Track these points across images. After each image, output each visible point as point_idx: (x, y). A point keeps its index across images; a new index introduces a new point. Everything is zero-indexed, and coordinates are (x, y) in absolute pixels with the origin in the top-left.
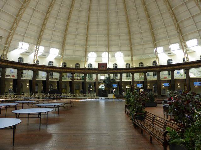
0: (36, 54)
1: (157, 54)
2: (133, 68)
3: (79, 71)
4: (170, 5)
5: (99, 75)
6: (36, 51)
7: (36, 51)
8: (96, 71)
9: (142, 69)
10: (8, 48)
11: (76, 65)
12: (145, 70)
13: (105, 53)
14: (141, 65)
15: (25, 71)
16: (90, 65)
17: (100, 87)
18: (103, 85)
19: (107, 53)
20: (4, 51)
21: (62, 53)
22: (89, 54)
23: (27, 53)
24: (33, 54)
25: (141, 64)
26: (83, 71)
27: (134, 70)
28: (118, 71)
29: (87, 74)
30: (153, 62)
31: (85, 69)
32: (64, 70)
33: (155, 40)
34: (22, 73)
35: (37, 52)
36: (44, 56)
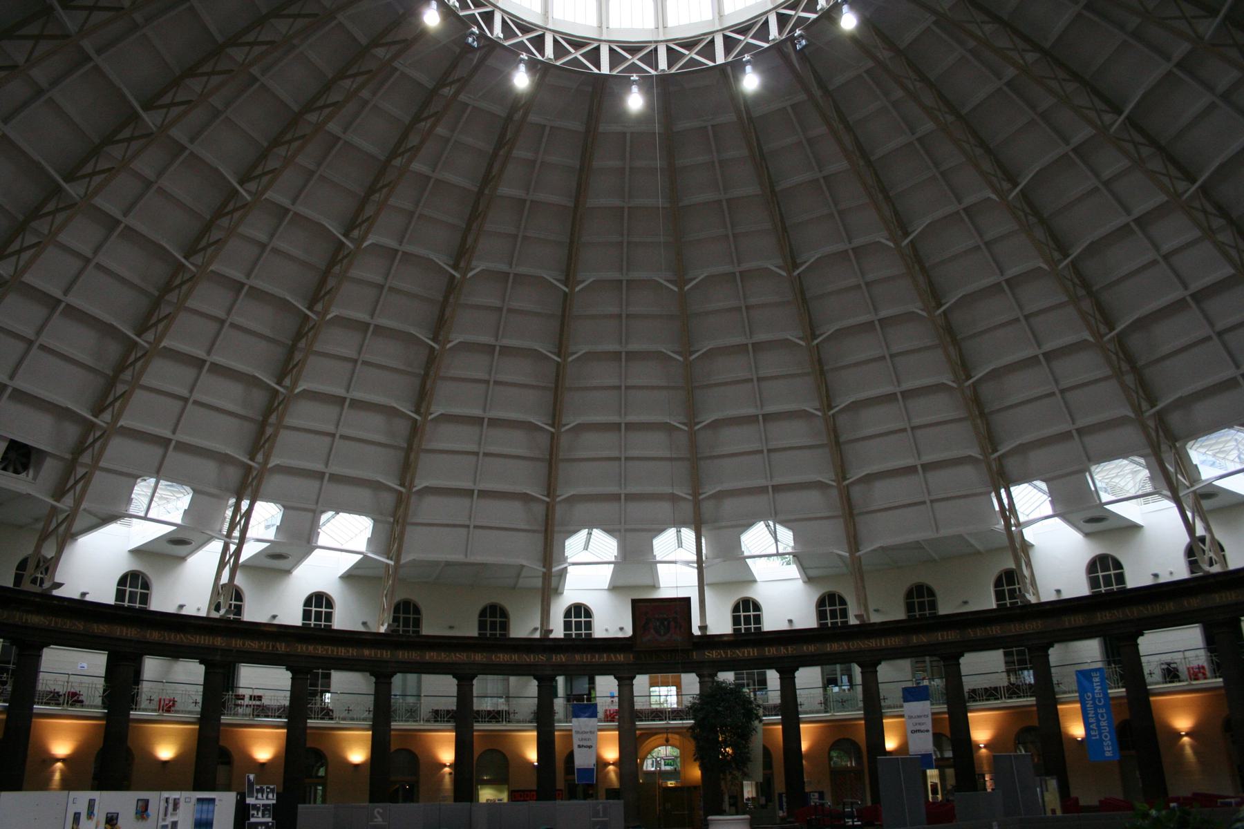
0: (233, 548)
1: (1018, 524)
2: (866, 630)
3: (503, 658)
4: (931, 284)
5: (641, 681)
6: (229, 535)
7: (229, 535)
8: (621, 658)
10: (71, 517)
11: (483, 613)
12: (951, 636)
15: (152, 666)
16: (579, 612)
17: (649, 766)
20: (44, 537)
22: (568, 543)
23: (177, 545)
24: (216, 547)
27: (873, 643)
28: (770, 651)
29: (560, 680)
31: (545, 645)
32: (402, 655)
34: (137, 677)
35: (236, 533)
36: (277, 562)
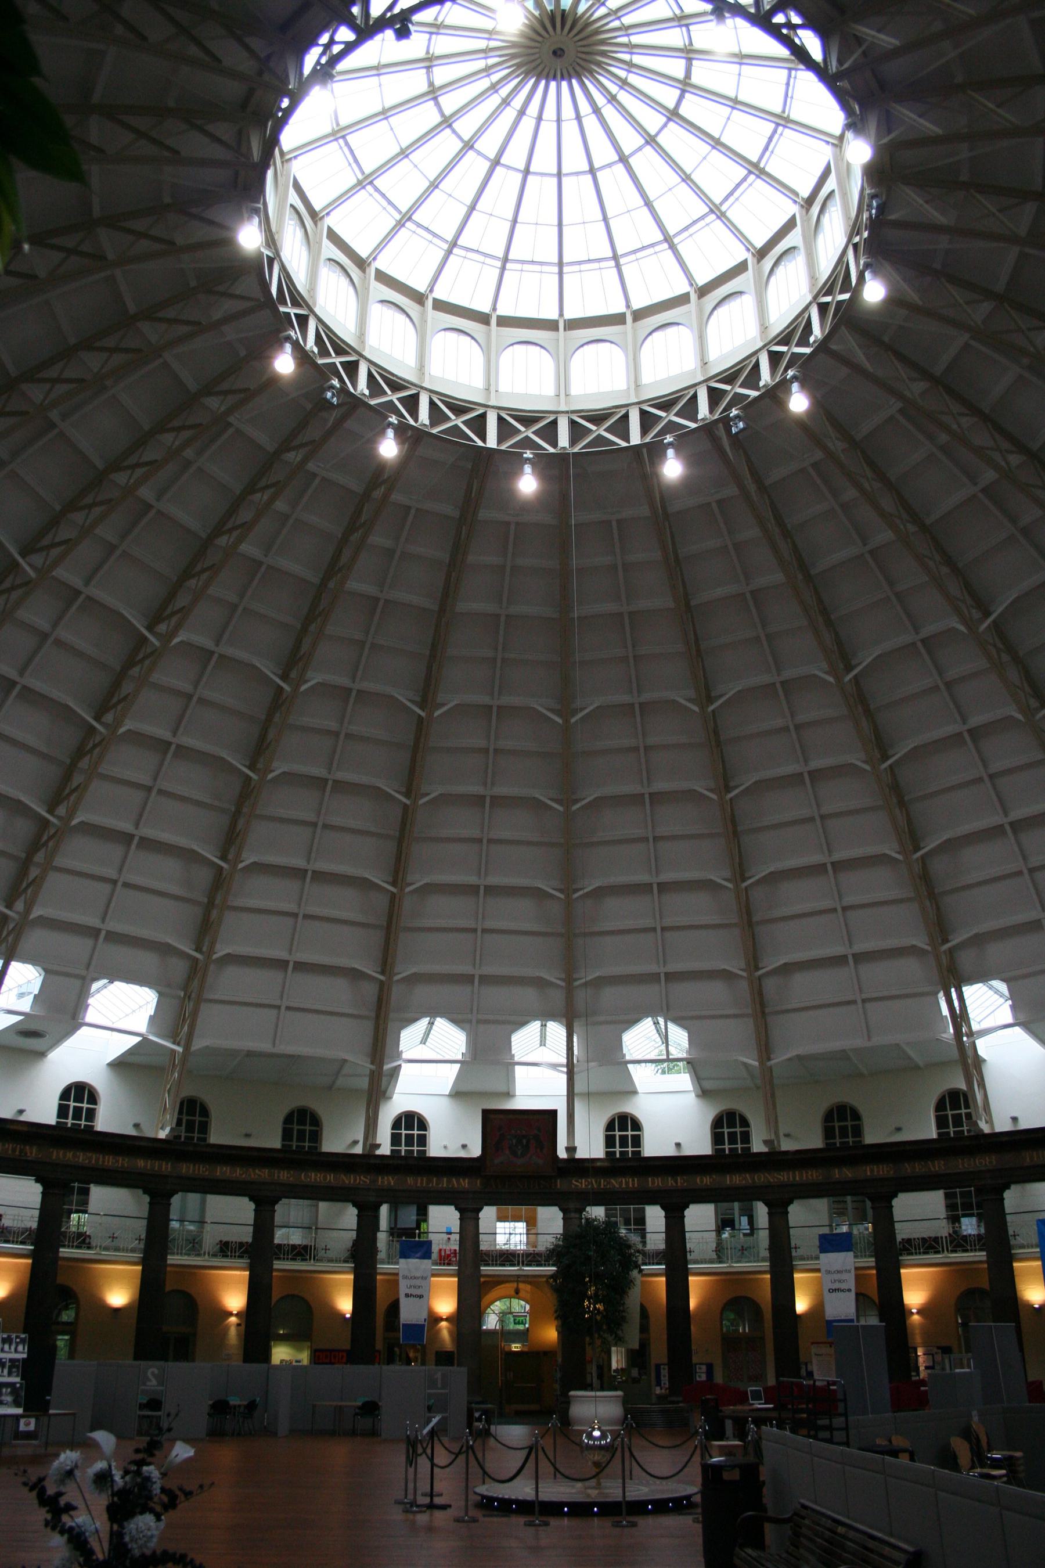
1: (971, 1034)
2: (775, 1159)
3: (315, 1177)
8: (465, 1183)
9: (854, 1169)
11: (288, 1119)
19: (556, 1031)
21: (180, 1012)
26: (348, 1180)
27: (784, 1177)
28: (655, 1183)
31: (368, 1162)
32: (186, 1169)
33: (940, 928)
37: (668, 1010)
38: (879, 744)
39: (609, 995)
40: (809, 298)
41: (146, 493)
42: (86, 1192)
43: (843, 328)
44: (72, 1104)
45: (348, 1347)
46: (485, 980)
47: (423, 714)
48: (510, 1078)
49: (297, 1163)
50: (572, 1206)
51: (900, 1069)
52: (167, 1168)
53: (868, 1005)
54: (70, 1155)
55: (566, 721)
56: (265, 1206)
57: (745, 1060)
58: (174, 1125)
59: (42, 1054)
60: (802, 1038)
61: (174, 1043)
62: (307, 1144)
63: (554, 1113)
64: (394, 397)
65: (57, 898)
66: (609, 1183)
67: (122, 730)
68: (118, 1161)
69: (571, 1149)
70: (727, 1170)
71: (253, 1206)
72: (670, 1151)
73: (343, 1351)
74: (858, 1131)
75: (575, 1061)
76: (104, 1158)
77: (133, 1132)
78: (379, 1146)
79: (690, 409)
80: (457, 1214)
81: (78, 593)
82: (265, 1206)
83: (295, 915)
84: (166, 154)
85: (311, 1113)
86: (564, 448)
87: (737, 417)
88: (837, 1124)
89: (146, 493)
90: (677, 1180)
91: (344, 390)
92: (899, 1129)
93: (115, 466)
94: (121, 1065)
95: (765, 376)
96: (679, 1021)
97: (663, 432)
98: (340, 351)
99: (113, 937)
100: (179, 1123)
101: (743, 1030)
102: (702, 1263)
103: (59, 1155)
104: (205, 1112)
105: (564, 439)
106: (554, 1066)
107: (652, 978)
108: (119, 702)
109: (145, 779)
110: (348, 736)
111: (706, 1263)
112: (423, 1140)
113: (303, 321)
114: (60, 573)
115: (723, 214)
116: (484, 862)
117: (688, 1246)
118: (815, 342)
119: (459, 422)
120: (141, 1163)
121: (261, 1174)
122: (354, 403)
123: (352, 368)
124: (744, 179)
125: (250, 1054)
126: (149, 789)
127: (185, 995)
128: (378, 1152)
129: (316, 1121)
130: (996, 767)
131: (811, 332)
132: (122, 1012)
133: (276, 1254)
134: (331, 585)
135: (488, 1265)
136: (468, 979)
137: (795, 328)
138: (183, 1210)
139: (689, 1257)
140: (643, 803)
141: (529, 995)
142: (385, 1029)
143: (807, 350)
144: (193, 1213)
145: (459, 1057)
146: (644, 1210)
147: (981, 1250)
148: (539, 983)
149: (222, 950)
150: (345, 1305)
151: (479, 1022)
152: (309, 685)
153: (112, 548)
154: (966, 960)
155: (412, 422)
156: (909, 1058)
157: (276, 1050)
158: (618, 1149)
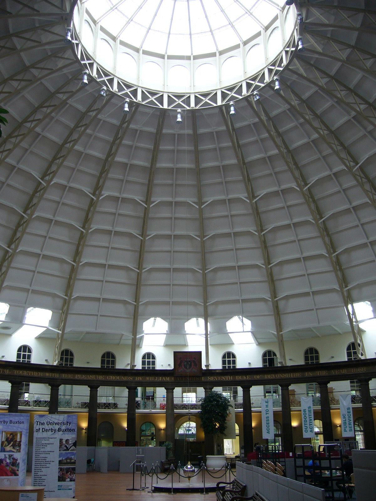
1: (357, 322)
2: (285, 369)
3: (112, 378)
8: (168, 379)
9: (317, 372)
11: (103, 356)
12: (324, 373)
13: (194, 320)
14: (312, 357)
16: (149, 356)
17: (181, 431)
18: (193, 424)
19: (202, 321)
21: (61, 319)
25: (229, 357)
26: (125, 379)
27: (286, 376)
28: (239, 378)
30: (349, 348)
31: (133, 372)
32: (64, 376)
33: (344, 281)
37: (243, 313)
38: (319, 213)
39: (221, 308)
40: (282, 49)
41: (38, 129)
42: (29, 385)
43: (295, 59)
44: (22, 353)
45: (125, 440)
46: (174, 303)
47: (146, 206)
48: (185, 340)
49: (107, 372)
50: (208, 387)
51: (333, 335)
52: (57, 376)
53: (318, 311)
54: (21, 372)
55: (200, 207)
56: (94, 389)
57: (273, 332)
58: (59, 360)
59: (10, 335)
60: (292, 324)
61: (59, 330)
62: (110, 365)
63: (200, 353)
64: (128, 91)
65: (13, 277)
66: (221, 378)
67: (34, 216)
68: (39, 374)
69: (207, 366)
70: (270, 372)
71: (89, 389)
72: (247, 366)
73: (124, 442)
74: (317, 358)
75: (209, 333)
76: (34, 373)
77: (45, 363)
78: (135, 366)
79: (239, 91)
80: (165, 391)
81: (15, 167)
82: (94, 389)
83: (102, 281)
84: (35, 12)
85: (112, 354)
86: (193, 107)
87: (256, 94)
88: (309, 355)
89: (38, 129)
90: (248, 378)
91: (108, 90)
92: (333, 357)
93: (25, 121)
94: (40, 338)
95: (267, 79)
96: (247, 317)
97: (229, 100)
98: (106, 75)
99: (34, 292)
100: (62, 359)
101: (271, 321)
102: (257, 408)
103: (17, 372)
104: (72, 354)
105: (193, 104)
106: (201, 335)
107: (237, 301)
108: (32, 206)
109: (44, 234)
110: (119, 214)
111: (258, 408)
112: (154, 363)
113: (91, 65)
114: (8, 160)
115: (251, 14)
116: (172, 259)
117: (251, 402)
118: (283, 66)
119: (153, 99)
120: (47, 374)
121: (91, 377)
122: (113, 95)
123: (111, 81)
124: (244, 15)
125: (88, 333)
126: (45, 237)
127: (62, 312)
128: (136, 368)
129: (113, 357)
130: (364, 221)
131: (282, 62)
132: (39, 319)
133: (98, 406)
134: (109, 159)
135: (177, 409)
136: (167, 303)
137: (258, 75)
138: (65, 390)
139: (252, 406)
140: (231, 236)
141: (191, 308)
142: (137, 323)
143: (281, 69)
144: (68, 393)
145: (166, 332)
146: (237, 388)
147: (360, 403)
148: (195, 304)
149: (75, 295)
150: (125, 425)
151: (172, 319)
152: (103, 196)
153: (26, 150)
154: (354, 293)
155: (135, 100)
156: (335, 330)
157: (97, 331)
158: (227, 365)
